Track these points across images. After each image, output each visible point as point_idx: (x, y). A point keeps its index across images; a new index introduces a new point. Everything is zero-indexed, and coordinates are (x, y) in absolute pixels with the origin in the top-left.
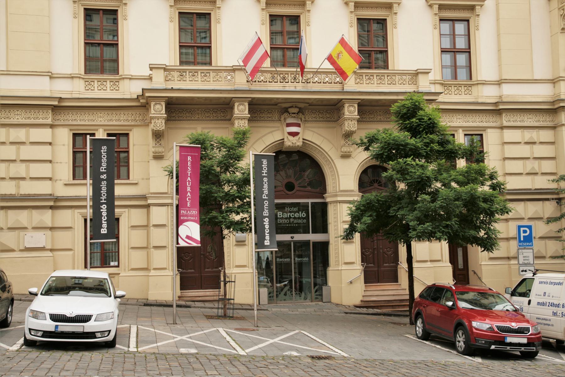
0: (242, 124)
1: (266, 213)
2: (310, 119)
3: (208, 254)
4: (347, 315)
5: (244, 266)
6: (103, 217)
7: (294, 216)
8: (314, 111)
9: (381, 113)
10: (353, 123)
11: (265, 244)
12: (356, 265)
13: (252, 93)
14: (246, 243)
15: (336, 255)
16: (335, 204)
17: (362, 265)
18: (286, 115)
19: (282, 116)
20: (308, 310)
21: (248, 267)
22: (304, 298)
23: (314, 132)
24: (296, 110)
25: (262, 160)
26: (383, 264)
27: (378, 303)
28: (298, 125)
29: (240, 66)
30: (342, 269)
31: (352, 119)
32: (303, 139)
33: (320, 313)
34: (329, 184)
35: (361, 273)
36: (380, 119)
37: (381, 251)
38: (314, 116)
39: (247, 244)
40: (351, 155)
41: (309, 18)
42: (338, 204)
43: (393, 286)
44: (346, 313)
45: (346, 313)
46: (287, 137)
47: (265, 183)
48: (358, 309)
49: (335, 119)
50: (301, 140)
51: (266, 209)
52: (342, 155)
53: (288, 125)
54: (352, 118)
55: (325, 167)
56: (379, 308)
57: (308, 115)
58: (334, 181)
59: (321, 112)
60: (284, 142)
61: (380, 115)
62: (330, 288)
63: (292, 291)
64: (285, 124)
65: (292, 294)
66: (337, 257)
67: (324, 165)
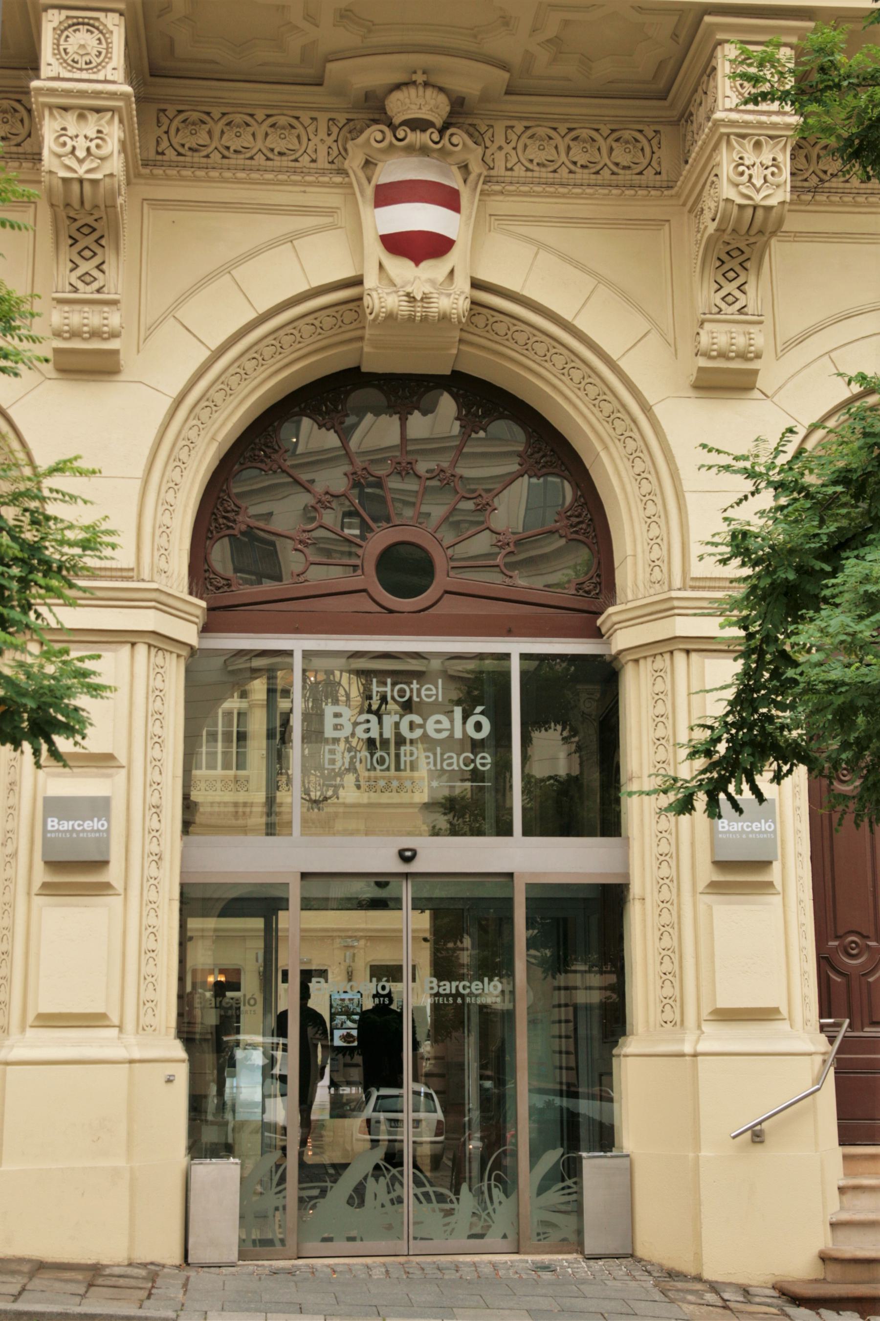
0: (81, 146)
2: (519, 171)
7: (418, 733)
8: (541, 131)
10: (766, 157)
12: (784, 1026)
14: (113, 874)
15: (667, 966)
16: (659, 663)
17: (822, 1028)
18: (374, 133)
19: (350, 145)
21: (120, 1027)
23: (541, 245)
30: (701, 1048)
32: (476, 284)
34: (629, 552)
35: (819, 1080)
39: (118, 884)
40: (755, 372)
42: (680, 657)
46: (381, 266)
49: (664, 176)
50: (462, 284)
52: (701, 370)
54: (761, 125)
55: (603, 455)
57: (508, 148)
58: (655, 531)
59: (584, 133)
60: (360, 299)
62: (631, 1171)
63: (396, 1181)
64: (370, 191)
65: (400, 1200)
67: (599, 447)
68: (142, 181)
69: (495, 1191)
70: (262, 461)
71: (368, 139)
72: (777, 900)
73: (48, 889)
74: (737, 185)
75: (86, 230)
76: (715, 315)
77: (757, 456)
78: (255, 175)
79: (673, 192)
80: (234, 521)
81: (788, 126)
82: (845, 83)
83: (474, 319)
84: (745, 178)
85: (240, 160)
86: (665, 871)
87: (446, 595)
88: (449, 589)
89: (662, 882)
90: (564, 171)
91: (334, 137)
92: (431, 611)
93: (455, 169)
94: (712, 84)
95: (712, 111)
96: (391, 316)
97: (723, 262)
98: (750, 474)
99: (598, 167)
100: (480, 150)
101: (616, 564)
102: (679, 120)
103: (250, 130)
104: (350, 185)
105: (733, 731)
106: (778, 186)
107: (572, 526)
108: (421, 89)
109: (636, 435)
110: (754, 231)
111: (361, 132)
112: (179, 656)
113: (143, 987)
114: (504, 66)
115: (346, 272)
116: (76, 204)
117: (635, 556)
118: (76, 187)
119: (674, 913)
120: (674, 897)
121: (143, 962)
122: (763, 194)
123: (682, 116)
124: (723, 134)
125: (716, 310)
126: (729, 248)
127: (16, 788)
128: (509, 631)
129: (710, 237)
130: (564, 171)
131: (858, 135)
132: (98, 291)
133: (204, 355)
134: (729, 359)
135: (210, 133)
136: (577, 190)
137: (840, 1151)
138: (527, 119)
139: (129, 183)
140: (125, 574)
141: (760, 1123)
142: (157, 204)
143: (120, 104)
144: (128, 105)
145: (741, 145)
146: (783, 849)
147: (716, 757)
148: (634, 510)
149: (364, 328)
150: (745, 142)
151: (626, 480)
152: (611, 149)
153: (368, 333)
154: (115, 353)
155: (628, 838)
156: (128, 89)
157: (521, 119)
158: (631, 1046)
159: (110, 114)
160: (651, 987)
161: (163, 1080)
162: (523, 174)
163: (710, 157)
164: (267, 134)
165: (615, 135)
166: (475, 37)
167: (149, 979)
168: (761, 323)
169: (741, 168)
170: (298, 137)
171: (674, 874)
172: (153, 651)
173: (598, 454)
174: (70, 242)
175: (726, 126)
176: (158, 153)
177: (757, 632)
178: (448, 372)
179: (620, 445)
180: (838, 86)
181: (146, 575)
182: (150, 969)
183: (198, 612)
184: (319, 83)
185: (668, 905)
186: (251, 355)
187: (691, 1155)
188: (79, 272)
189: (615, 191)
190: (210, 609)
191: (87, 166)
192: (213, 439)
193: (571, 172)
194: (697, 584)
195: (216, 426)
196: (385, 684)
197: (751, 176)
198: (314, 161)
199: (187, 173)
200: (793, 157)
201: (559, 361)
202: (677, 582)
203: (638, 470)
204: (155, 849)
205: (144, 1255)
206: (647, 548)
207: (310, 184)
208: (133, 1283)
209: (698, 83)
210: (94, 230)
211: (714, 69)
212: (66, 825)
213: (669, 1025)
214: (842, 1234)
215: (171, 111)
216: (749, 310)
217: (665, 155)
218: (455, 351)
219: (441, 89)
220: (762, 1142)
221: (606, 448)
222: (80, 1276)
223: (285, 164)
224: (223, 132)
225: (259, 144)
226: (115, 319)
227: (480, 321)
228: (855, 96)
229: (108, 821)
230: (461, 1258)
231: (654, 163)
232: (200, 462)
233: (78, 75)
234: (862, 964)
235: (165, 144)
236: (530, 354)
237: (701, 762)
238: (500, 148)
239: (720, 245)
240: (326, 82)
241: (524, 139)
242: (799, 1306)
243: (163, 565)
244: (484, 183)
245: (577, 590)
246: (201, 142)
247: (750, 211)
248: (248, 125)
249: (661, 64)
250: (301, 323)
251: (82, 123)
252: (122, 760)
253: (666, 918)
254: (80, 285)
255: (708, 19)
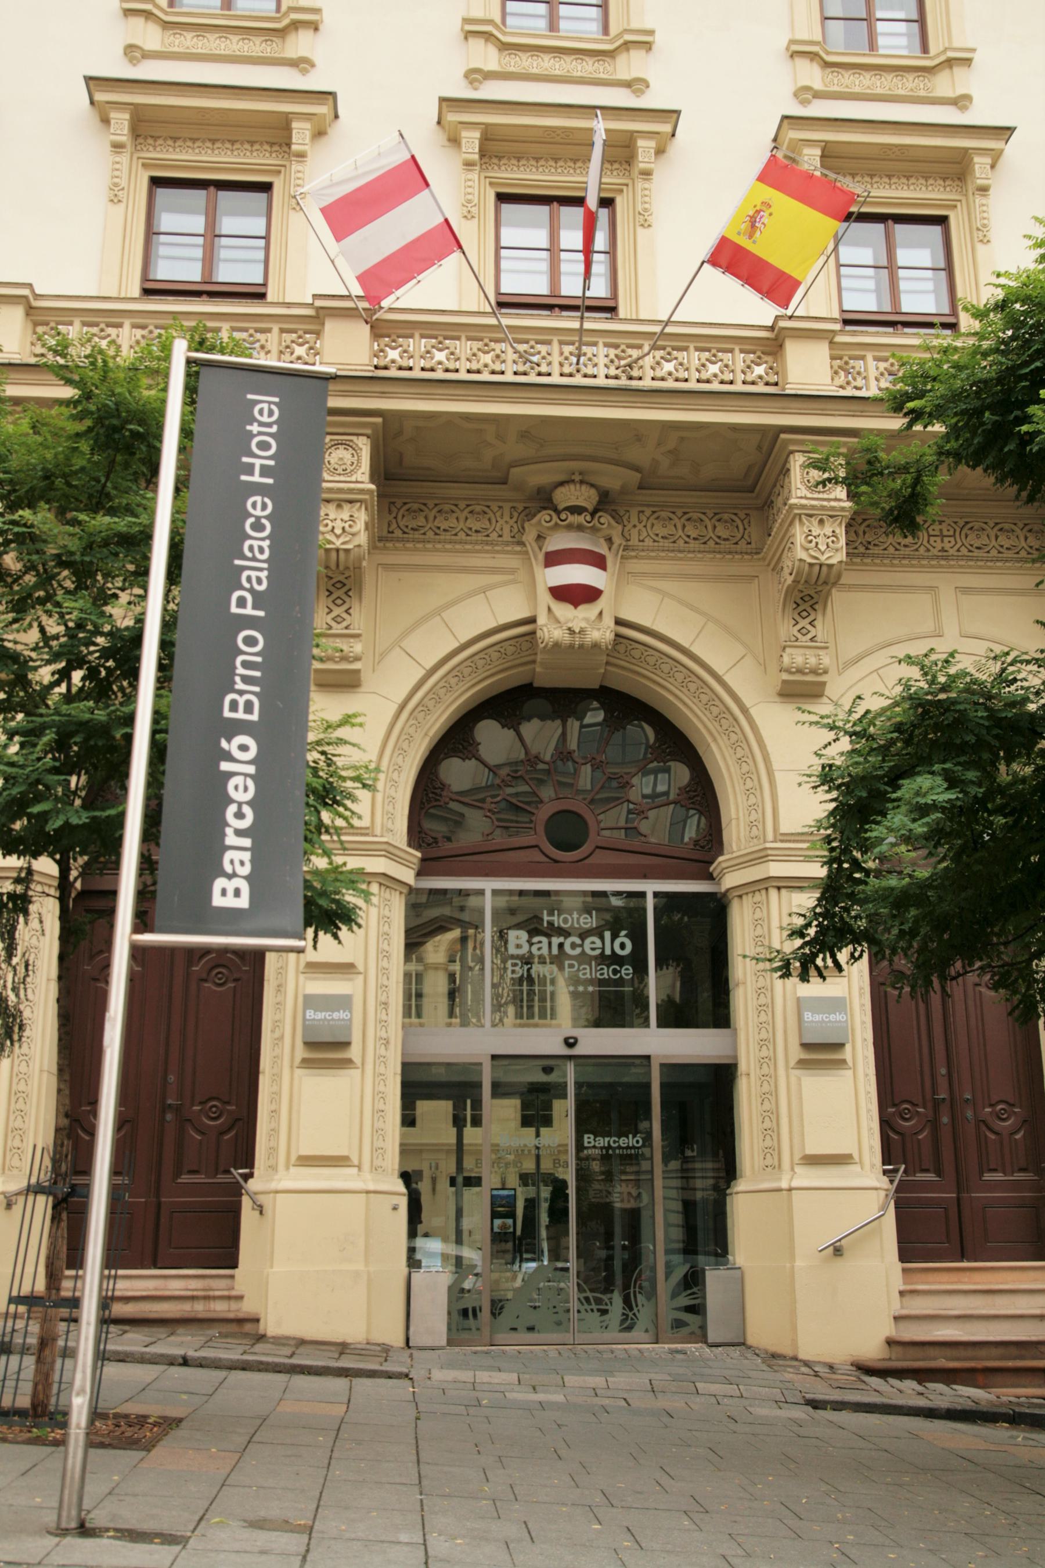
1: (241, 701)
2: (648, 542)
3: (197, 1108)
4: (821, 1412)
5: (339, 1161)
6: (232, 809)
7: (578, 950)
8: (663, 514)
9: (944, 526)
10: (828, 531)
11: (218, 901)
12: (856, 1168)
13: (383, 395)
14: (354, 1052)
15: (767, 1124)
16: (758, 897)
18: (544, 516)
19: (526, 525)
20: (620, 1380)
21: (359, 1167)
22: (623, 1322)
23: (665, 594)
24: (585, 497)
25: (250, 397)
26: (981, 1174)
27: (970, 1352)
28: (599, 562)
29: (348, 297)
30: (794, 1184)
31: (822, 516)
32: (619, 622)
33: (675, 1403)
34: (734, 816)
35: (884, 1208)
36: (943, 550)
37: (969, 1114)
38: (663, 532)
41: (647, 199)
42: (773, 893)
43: (1032, 1274)
44: (815, 1404)
45: (815, 1404)
46: (549, 609)
47: (258, 526)
48: (874, 1381)
49: (753, 545)
50: (609, 622)
51: (246, 679)
52: (784, 682)
53: (553, 559)
54: (823, 508)
55: (713, 746)
56: (980, 1378)
57: (640, 526)
58: (752, 800)
59: (695, 516)
60: (534, 633)
61: (942, 536)
64: (541, 557)
66: (772, 1132)
67: (709, 739)
68: (377, 551)
69: (639, 1296)
70: (461, 752)
71: (540, 521)
72: (850, 1073)
73: (307, 1063)
74: (807, 550)
75: (338, 585)
76: (792, 643)
77: (836, 715)
78: (458, 546)
79: (760, 556)
80: (441, 795)
81: (843, 509)
82: (886, 472)
83: (617, 647)
84: (813, 544)
85: (447, 536)
86: (765, 1052)
87: (598, 850)
88: (599, 845)
89: (761, 1061)
90: (681, 542)
91: (514, 519)
92: (586, 861)
93: (602, 541)
94: (787, 480)
95: (788, 499)
96: (557, 645)
97: (798, 605)
98: (832, 728)
99: (706, 539)
100: (620, 527)
101: (724, 825)
102: (763, 506)
103: (455, 515)
104: (527, 553)
105: (821, 919)
106: (837, 550)
107: (690, 798)
108: (578, 486)
109: (737, 730)
110: (820, 582)
111: (535, 515)
112: (401, 893)
113: (375, 1138)
114: (637, 469)
115: (524, 614)
116: (333, 566)
117: (738, 819)
118: (334, 555)
119: (772, 1084)
120: (772, 1071)
121: (376, 1119)
122: (826, 556)
123: (765, 503)
124: (796, 514)
125: (794, 639)
126: (802, 595)
127: (282, 989)
128: (645, 874)
129: (789, 587)
130: (681, 542)
131: (896, 507)
132: (346, 628)
133: (420, 673)
134: (804, 674)
135: (426, 518)
136: (691, 555)
137: (899, 1266)
138: (654, 506)
139: (369, 553)
140: (363, 831)
141: (840, 1240)
142: (388, 567)
143: (367, 497)
144: (372, 498)
145: (810, 522)
146: (853, 1035)
147: (807, 939)
148: (736, 785)
149: (536, 654)
150: (813, 519)
151: (730, 763)
152: (715, 527)
153: (539, 658)
154: (358, 672)
155: (736, 1029)
156: (373, 487)
157: (648, 506)
158: (741, 1185)
159: (358, 504)
160: (755, 1141)
161: (390, 1207)
162: (651, 544)
163: (787, 530)
164: (467, 518)
165: (717, 517)
166: (616, 449)
167: (380, 1132)
168: (827, 648)
169: (810, 538)
170: (489, 520)
171: (772, 1054)
172: (383, 888)
173: (709, 745)
174: (327, 593)
175: (798, 508)
176: (389, 532)
177: (837, 847)
178: (597, 687)
179: (725, 738)
180: (881, 474)
181: (378, 831)
182: (380, 1124)
183: (415, 861)
184: (505, 483)
185: (767, 1078)
186: (454, 673)
187: (788, 1265)
188: (333, 615)
189: (718, 556)
190: (423, 860)
191: (342, 540)
192: (426, 734)
193: (686, 542)
194: (785, 838)
195: (429, 724)
196: (548, 922)
197: (817, 543)
198: (500, 536)
199: (410, 545)
200: (847, 533)
201: (680, 677)
202: (770, 836)
203: (739, 756)
204: (384, 1035)
205: (379, 1337)
206: (747, 813)
207: (498, 552)
208: (372, 1353)
209: (777, 481)
210: (345, 585)
211: (788, 470)
212: (320, 1015)
213: (769, 1169)
214: (902, 1325)
215: (399, 502)
216: (819, 638)
217: (754, 532)
218: (602, 671)
219: (592, 485)
220: (841, 1255)
221: (715, 740)
222: (333, 1348)
223: (480, 538)
224: (435, 517)
225: (461, 525)
226: (358, 648)
227: (621, 648)
228: (893, 480)
229: (351, 1012)
230: (614, 1346)
231: (746, 536)
232: (417, 751)
233: (337, 478)
234: (912, 1126)
235: (394, 526)
236: (658, 672)
237: (798, 942)
238: (635, 526)
239: (796, 592)
240: (510, 481)
241: (652, 520)
242: (871, 1376)
243: (390, 825)
244: (624, 550)
245: (695, 845)
246: (420, 524)
247: (817, 568)
248: (453, 512)
249: (750, 468)
250: (490, 650)
251: (340, 511)
252: (361, 968)
253: (766, 1088)
254: (333, 624)
255: (783, 436)
